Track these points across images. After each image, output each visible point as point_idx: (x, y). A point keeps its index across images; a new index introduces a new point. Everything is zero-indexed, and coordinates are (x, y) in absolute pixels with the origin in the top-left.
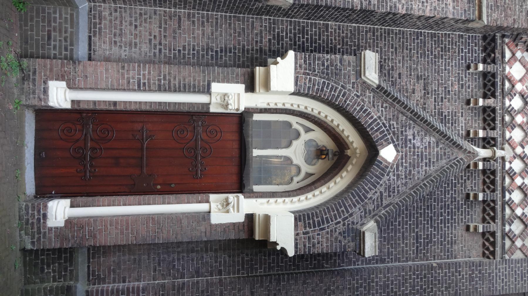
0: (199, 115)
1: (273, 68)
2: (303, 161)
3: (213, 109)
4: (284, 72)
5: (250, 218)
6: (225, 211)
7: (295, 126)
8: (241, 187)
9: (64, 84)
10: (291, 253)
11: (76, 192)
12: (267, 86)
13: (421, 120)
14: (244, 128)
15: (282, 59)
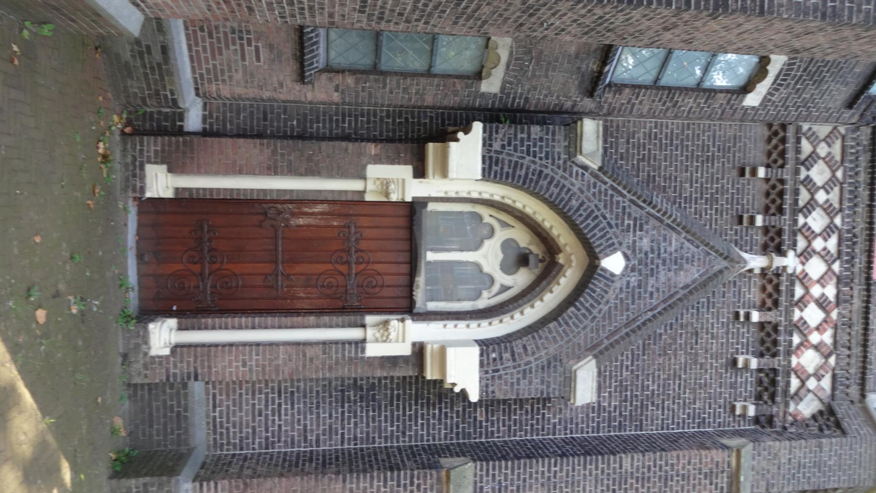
0: (351, 207)
1: (453, 145)
2: (498, 268)
3: (368, 198)
4: (467, 150)
5: (419, 350)
6: (390, 339)
7: (487, 219)
8: (407, 308)
9: (165, 167)
10: (474, 397)
11: (190, 312)
12: (444, 172)
13: (664, 215)
14: (414, 293)
15: (466, 133)
